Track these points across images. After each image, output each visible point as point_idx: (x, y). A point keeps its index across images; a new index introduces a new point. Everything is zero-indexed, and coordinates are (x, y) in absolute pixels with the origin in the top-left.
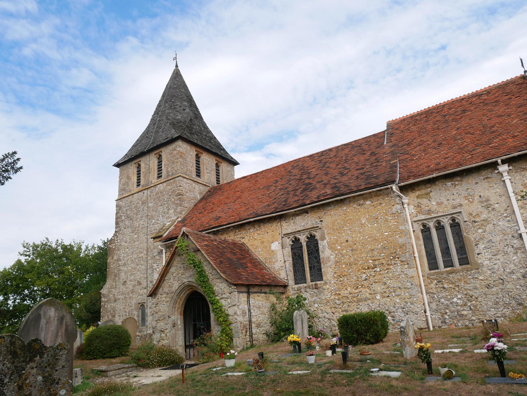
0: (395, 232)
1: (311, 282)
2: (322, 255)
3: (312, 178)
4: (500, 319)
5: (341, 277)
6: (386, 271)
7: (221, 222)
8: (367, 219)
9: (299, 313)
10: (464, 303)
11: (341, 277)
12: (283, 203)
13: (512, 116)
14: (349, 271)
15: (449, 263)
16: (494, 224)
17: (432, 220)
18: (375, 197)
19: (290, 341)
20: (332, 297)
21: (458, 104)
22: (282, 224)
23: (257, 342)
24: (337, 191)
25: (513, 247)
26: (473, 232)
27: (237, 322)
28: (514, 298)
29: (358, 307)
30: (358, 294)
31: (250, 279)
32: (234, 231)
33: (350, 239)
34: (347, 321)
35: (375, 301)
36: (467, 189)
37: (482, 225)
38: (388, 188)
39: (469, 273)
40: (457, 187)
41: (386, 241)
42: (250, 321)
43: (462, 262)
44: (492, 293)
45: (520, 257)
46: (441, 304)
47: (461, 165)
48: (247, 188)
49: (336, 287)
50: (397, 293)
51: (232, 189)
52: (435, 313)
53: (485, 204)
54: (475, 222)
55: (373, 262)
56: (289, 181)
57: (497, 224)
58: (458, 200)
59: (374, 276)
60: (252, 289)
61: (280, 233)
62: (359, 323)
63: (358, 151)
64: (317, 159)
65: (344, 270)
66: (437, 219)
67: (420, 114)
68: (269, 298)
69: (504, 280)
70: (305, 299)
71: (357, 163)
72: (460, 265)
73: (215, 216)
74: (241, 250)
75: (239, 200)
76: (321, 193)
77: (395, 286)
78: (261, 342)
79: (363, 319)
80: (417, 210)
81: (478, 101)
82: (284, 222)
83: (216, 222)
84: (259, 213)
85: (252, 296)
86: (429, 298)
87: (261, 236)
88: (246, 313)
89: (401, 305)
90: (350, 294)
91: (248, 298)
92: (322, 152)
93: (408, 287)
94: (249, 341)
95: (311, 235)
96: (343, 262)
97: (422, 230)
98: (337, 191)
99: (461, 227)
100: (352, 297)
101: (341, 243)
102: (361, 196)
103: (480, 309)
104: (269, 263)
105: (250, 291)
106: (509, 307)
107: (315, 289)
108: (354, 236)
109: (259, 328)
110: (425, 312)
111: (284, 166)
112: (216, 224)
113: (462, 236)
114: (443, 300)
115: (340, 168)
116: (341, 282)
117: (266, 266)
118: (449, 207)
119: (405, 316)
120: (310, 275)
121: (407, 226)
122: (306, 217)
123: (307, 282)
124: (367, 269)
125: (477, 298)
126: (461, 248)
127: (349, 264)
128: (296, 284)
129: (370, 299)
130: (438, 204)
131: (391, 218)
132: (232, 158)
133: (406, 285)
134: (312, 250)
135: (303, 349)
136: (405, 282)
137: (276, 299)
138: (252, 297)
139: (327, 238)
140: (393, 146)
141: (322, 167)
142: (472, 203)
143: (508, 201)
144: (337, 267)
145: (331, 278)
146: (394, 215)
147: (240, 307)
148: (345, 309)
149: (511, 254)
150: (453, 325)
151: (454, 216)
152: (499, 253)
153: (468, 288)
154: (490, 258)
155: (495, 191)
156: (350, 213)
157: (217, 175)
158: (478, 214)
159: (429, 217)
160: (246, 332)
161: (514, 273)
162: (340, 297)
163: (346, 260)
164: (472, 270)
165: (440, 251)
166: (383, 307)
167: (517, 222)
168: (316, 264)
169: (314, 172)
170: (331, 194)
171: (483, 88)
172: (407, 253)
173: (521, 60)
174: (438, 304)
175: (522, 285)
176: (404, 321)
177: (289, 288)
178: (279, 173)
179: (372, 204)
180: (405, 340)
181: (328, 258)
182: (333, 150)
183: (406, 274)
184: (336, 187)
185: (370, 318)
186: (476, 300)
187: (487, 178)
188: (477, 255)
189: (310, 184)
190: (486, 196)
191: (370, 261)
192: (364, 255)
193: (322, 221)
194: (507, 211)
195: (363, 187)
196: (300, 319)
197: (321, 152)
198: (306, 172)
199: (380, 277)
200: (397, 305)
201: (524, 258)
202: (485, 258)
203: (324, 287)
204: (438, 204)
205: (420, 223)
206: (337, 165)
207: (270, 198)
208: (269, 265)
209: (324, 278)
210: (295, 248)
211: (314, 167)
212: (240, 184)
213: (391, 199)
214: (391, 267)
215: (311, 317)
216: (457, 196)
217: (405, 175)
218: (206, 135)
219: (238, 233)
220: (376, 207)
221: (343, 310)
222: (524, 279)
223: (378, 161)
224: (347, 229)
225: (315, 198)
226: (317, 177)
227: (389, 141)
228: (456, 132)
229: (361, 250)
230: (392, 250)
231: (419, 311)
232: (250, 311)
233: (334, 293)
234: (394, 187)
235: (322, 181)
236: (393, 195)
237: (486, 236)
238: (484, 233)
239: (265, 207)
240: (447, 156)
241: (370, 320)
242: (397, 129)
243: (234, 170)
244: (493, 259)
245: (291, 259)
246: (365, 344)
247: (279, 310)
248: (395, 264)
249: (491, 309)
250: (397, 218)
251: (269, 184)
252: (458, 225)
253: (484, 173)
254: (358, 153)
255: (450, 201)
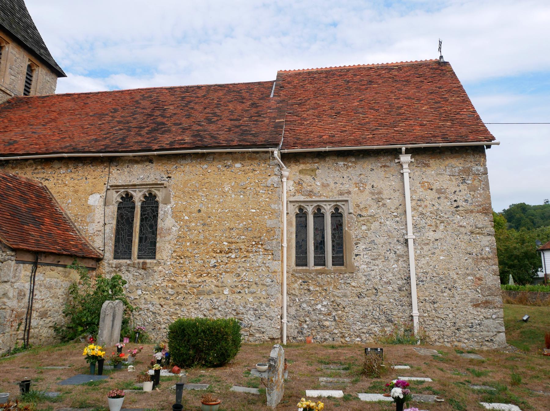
0: (265, 211)
1: (138, 258)
2: (160, 224)
3: (168, 117)
4: (365, 336)
5: (182, 258)
6: (243, 260)
7: (16, 149)
8: (232, 187)
9: (111, 304)
10: (329, 312)
11: (182, 258)
12: (119, 142)
13: (422, 102)
14: (194, 252)
15: (320, 261)
16: (380, 223)
17: (312, 204)
18: (249, 160)
19: (87, 354)
20: (164, 284)
21: (364, 73)
22: (111, 170)
23: (35, 339)
24: (199, 140)
25: (395, 253)
26: (356, 228)
27: (5, 309)
28: (384, 312)
29: (197, 301)
30: (201, 284)
31: (42, 242)
32: (35, 167)
33: (203, 209)
34: (184, 330)
35: (221, 296)
36: (361, 174)
37: (368, 221)
38: (267, 152)
39: (342, 276)
40: (349, 169)
41: (250, 220)
42: (30, 309)
43: (336, 261)
44: (362, 304)
45: (401, 266)
46: (301, 310)
47: (360, 144)
48: (70, 110)
49: (172, 270)
50: (251, 290)
51: (45, 107)
52: (292, 320)
53: (377, 196)
54: (360, 216)
55: (228, 245)
56: (134, 115)
57: (384, 224)
58: (347, 186)
59: (227, 263)
60: (43, 258)
61: (106, 183)
62: (200, 334)
63: (236, 98)
64: (179, 94)
65: (188, 249)
66: (318, 204)
67: (319, 72)
68: (70, 274)
69: (379, 290)
70: (124, 283)
71: (232, 112)
72: (333, 265)
73: (7, 139)
74: (38, 196)
75: (53, 123)
76: (177, 139)
77: (251, 280)
78: (44, 340)
79: (208, 330)
80: (296, 188)
81: (387, 75)
82: (114, 168)
83: (8, 148)
84: (80, 147)
85: (40, 269)
86: (289, 301)
87: (76, 181)
88: (25, 295)
89: (254, 305)
90: (189, 283)
91: (34, 271)
92: (188, 87)
93: (267, 284)
94: (21, 339)
95: (150, 194)
96: (188, 238)
97: (297, 214)
98: (199, 140)
99: (343, 219)
100: (191, 287)
101: (191, 213)
102: (231, 155)
103: (345, 321)
104: (81, 223)
105: (39, 261)
106: (377, 323)
107: (143, 269)
108: (210, 205)
109: (44, 319)
110: (281, 318)
111: (131, 93)
112: (6, 150)
113: (342, 230)
114: (304, 305)
115: (208, 113)
116: (181, 265)
117: (75, 227)
118: (336, 191)
119: (256, 320)
120: (139, 249)
121: (280, 206)
122: (149, 167)
123: (132, 258)
124: (218, 253)
125: (344, 308)
126: (338, 244)
127: (195, 242)
128: (115, 258)
129: (214, 293)
130: (324, 186)
131: (264, 192)
132: (57, 65)
133: (264, 281)
134: (148, 214)
135: (107, 365)
136: (264, 277)
137: (80, 277)
138: (42, 270)
139: (173, 203)
140: (281, 102)
141: (184, 107)
142: (362, 192)
143: (401, 198)
144: (179, 244)
145: (167, 258)
146: (268, 188)
147: (16, 285)
148: (180, 301)
149: (392, 261)
150: (311, 337)
151: (338, 203)
152: (380, 258)
153: (337, 294)
154: (368, 262)
155: (390, 184)
156: (212, 174)
157: (26, 82)
158: (366, 208)
159: (309, 199)
160: (20, 325)
161: (390, 284)
162: (175, 284)
163: (193, 236)
164: (346, 273)
165: (313, 244)
166: (230, 305)
167: (406, 224)
168: (150, 235)
169: (171, 109)
170: (191, 143)
171: (394, 62)
172: (274, 241)
173: (440, 43)
174: (299, 309)
175: (396, 299)
176: (275, 349)
177: (105, 263)
178: (121, 101)
179: (243, 169)
180: (274, 379)
181: (169, 230)
182: (203, 88)
183: (268, 267)
184: (199, 135)
185: (218, 329)
186: (343, 310)
187: (385, 166)
188: (354, 257)
189: (164, 124)
190: (379, 187)
191: (224, 243)
192: (218, 234)
193: (170, 177)
194: (398, 210)
195: (235, 143)
196: (112, 314)
197: (186, 87)
198: (160, 108)
199: (233, 265)
200: (249, 305)
201: (405, 267)
202: (363, 261)
203: (155, 268)
204: (323, 185)
205: (297, 205)
206: (205, 108)
207: (101, 131)
208: (80, 225)
209: (158, 256)
210: (124, 208)
211: (173, 104)
212: (60, 103)
213: (268, 166)
214: (251, 255)
215: (128, 310)
216: (347, 180)
217: (291, 140)
218: (20, 19)
219: (40, 171)
220: (247, 173)
221: (175, 303)
222: (400, 292)
223: (260, 116)
224: (203, 195)
225: (167, 144)
226: (175, 117)
227: (277, 94)
228: (358, 103)
229: (216, 226)
230: (256, 233)
231: (275, 316)
232: (33, 292)
233: (167, 279)
234: (276, 153)
235: (180, 124)
236: (271, 162)
237: (369, 235)
238: (367, 232)
239: (90, 141)
240: (344, 129)
241: (217, 333)
242: (289, 83)
243: (56, 83)
244: (372, 264)
245: (114, 222)
246: (203, 365)
247: (82, 293)
248: (256, 252)
249: (358, 323)
250: (270, 193)
251: (104, 112)
252: (341, 215)
253: (383, 159)
254: (235, 100)
255: (337, 185)
